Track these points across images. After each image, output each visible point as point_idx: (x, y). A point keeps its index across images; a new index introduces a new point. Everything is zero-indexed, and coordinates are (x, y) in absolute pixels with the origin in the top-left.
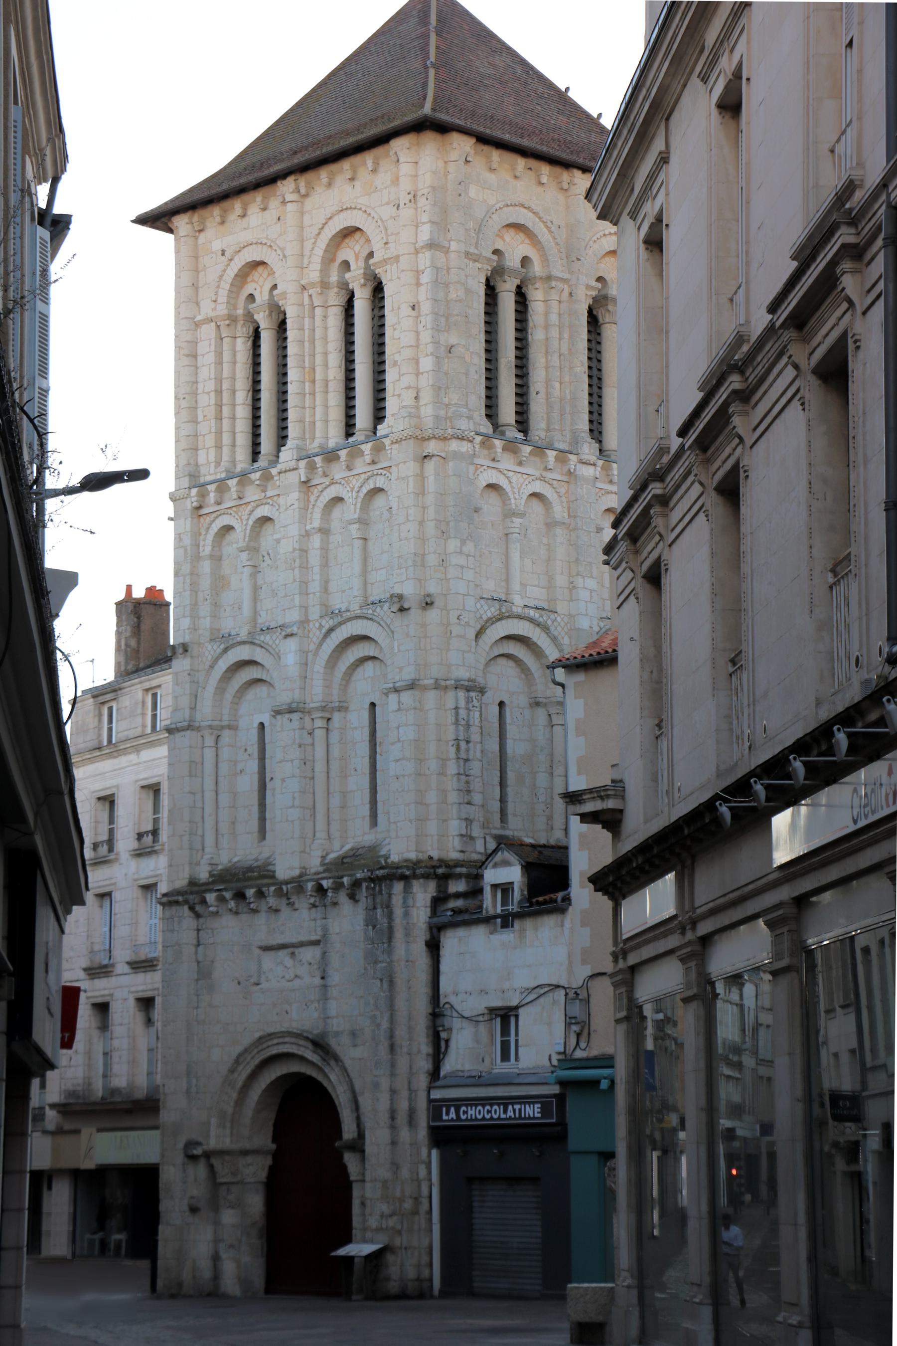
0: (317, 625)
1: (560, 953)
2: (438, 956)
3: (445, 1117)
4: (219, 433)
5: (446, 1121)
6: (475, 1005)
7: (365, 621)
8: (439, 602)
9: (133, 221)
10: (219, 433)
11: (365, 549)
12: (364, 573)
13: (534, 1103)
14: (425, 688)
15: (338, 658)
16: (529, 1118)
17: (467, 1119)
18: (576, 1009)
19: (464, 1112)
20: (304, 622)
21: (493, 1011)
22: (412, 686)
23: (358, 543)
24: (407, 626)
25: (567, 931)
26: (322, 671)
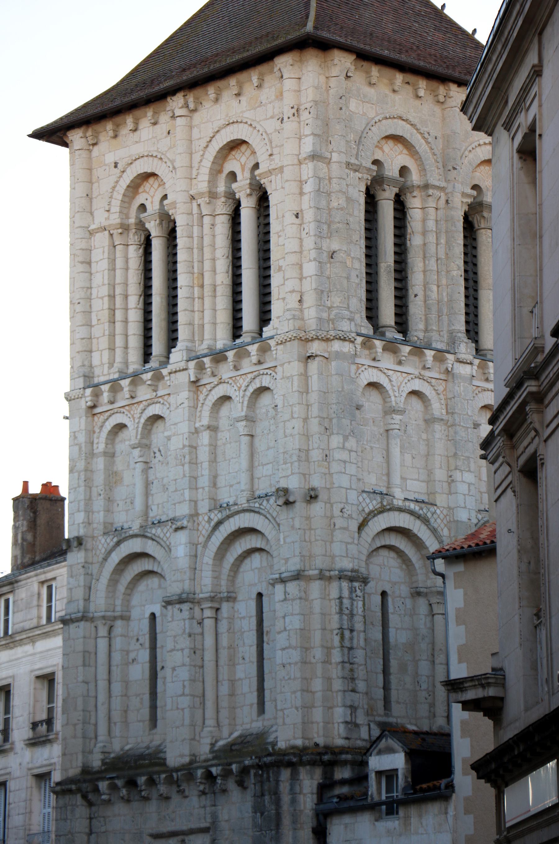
0: (206, 518)
4: (112, 336)
7: (252, 514)
8: (323, 496)
10: (112, 336)
11: (252, 445)
14: (310, 579)
15: (226, 550)
20: (194, 516)
22: (298, 576)
24: (293, 519)
26: (211, 562)
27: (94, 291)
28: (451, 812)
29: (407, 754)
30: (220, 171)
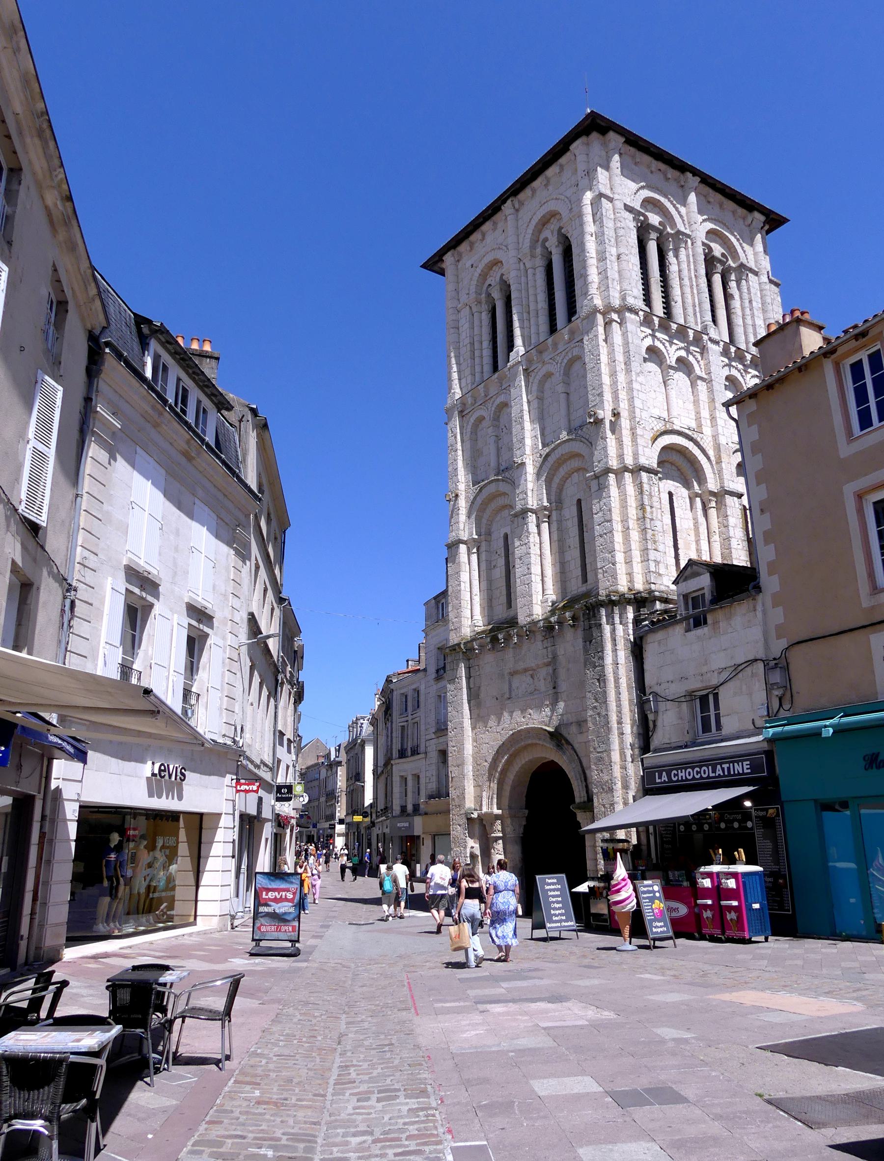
1: (756, 633)
2: (642, 658)
3: (658, 781)
4: (473, 367)
5: (659, 783)
6: (677, 689)
9: (424, 266)
10: (473, 367)
11: (568, 400)
12: (569, 414)
13: (742, 761)
16: (739, 774)
17: (678, 781)
18: (776, 677)
19: (675, 775)
21: (690, 696)
23: (563, 396)
25: (759, 614)
27: (461, 344)
28: (759, 608)
29: (711, 573)
30: (538, 241)
